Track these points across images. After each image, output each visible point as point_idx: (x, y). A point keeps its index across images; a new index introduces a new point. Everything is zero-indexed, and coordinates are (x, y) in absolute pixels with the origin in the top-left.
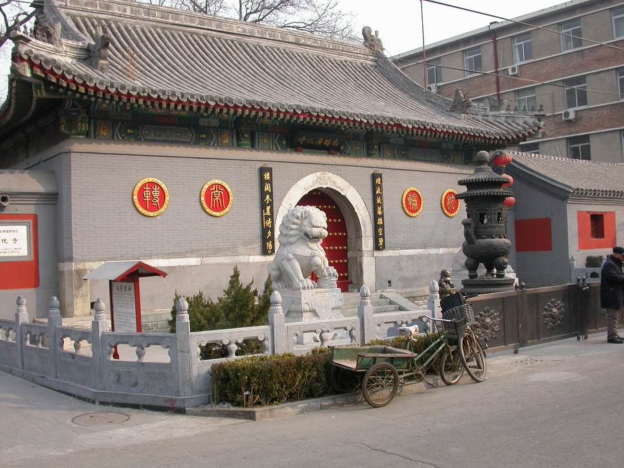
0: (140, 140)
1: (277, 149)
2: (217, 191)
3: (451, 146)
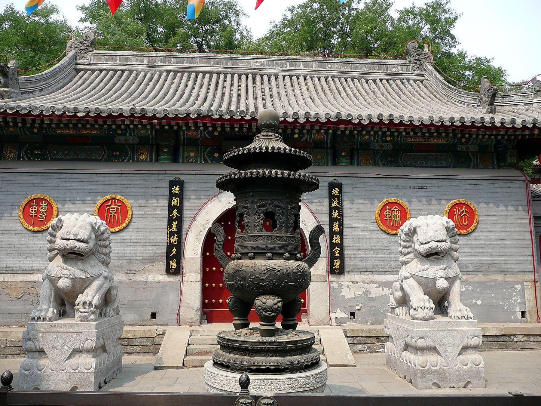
0: (47, 159)
1: (24, 159)
2: (113, 206)
3: (473, 148)
